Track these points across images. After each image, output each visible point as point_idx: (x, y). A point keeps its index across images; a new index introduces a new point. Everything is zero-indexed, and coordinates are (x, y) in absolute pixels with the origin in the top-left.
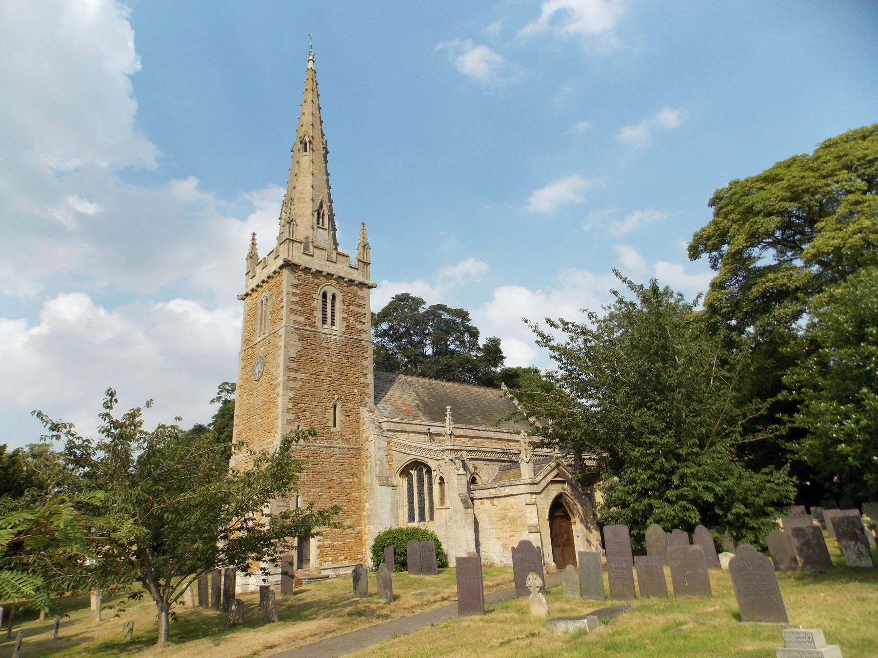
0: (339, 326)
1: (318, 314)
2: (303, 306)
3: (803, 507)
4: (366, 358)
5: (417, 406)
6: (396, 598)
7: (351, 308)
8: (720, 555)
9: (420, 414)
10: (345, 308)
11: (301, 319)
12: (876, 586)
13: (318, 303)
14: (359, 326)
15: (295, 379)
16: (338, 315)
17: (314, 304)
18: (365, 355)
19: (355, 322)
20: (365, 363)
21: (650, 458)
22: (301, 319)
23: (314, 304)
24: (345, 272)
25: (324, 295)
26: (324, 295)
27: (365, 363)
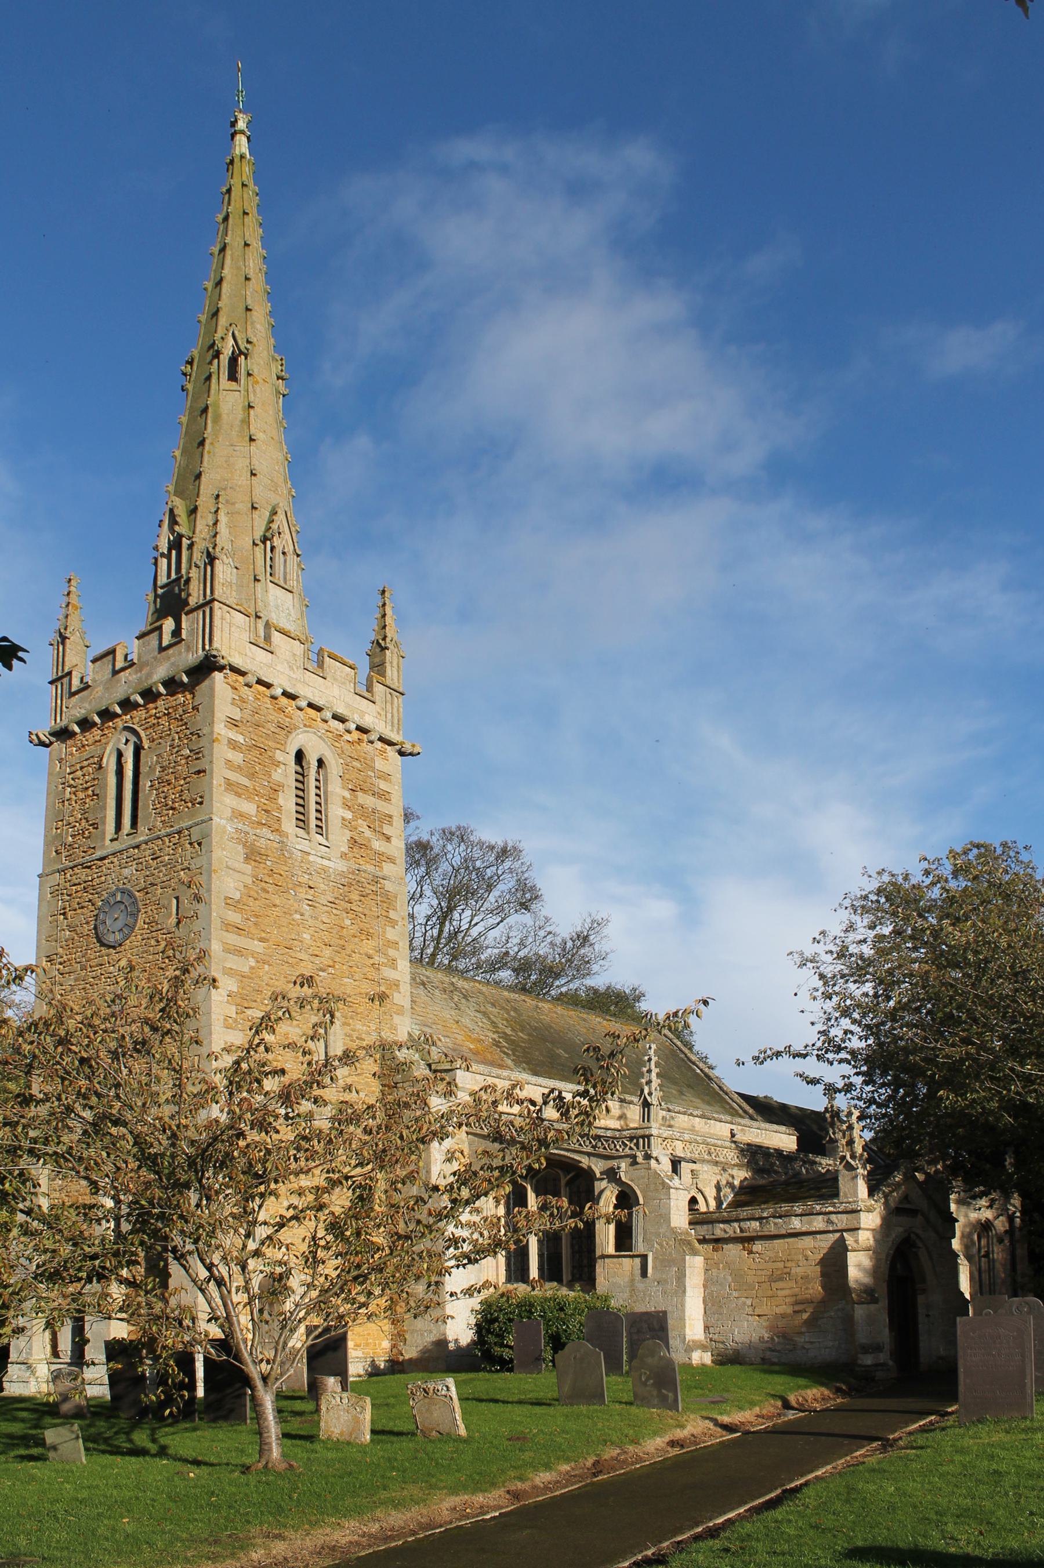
0: (340, 838)
1: (288, 801)
2: (252, 776)
3: (363, 442)
4: (393, 923)
5: (497, 1044)
6: (389, 1460)
7: (363, 798)
8: (323, 1436)
9: (509, 1062)
10: (347, 794)
11: (249, 808)
12: (975, 597)
13: (286, 773)
14: (377, 845)
15: (239, 952)
16: (337, 812)
17: (277, 775)
18: (392, 914)
19: (368, 833)
20: (391, 934)
21: (476, 920)
22: (249, 808)
23: (277, 775)
24: (348, 706)
25: (300, 756)
26: (300, 756)
27: (391, 934)
